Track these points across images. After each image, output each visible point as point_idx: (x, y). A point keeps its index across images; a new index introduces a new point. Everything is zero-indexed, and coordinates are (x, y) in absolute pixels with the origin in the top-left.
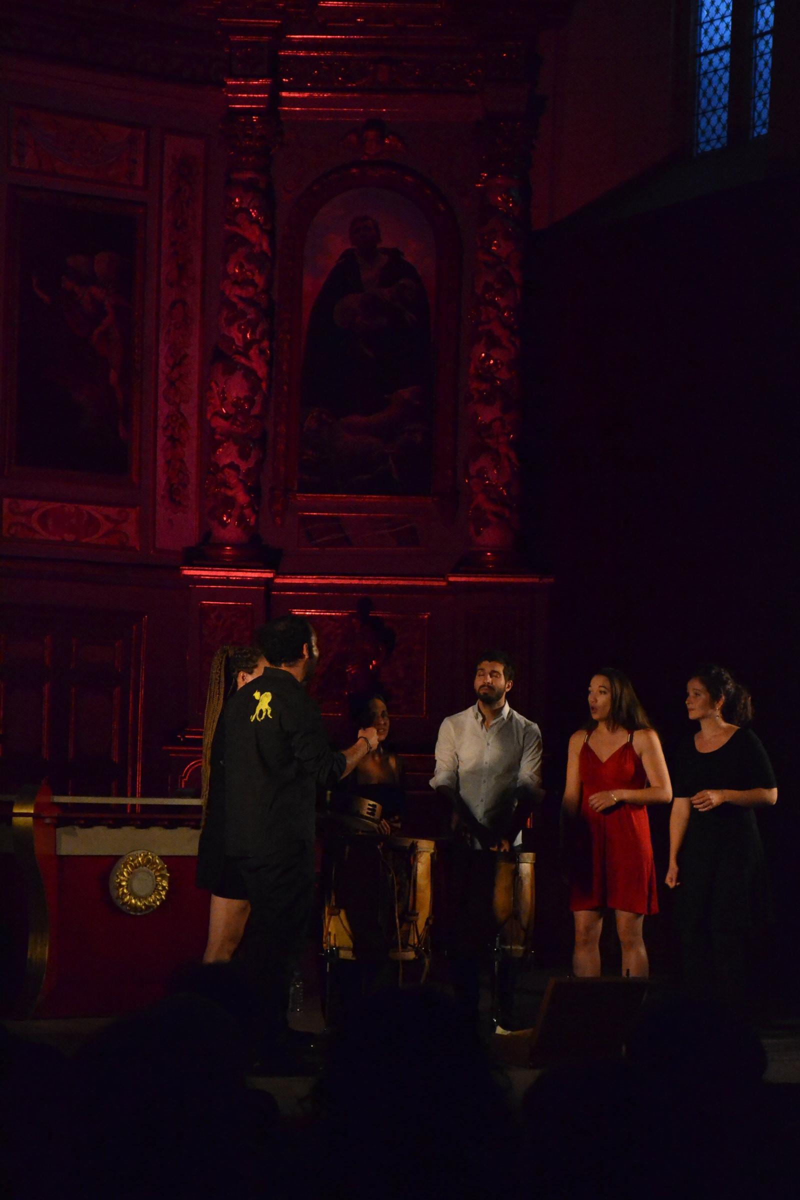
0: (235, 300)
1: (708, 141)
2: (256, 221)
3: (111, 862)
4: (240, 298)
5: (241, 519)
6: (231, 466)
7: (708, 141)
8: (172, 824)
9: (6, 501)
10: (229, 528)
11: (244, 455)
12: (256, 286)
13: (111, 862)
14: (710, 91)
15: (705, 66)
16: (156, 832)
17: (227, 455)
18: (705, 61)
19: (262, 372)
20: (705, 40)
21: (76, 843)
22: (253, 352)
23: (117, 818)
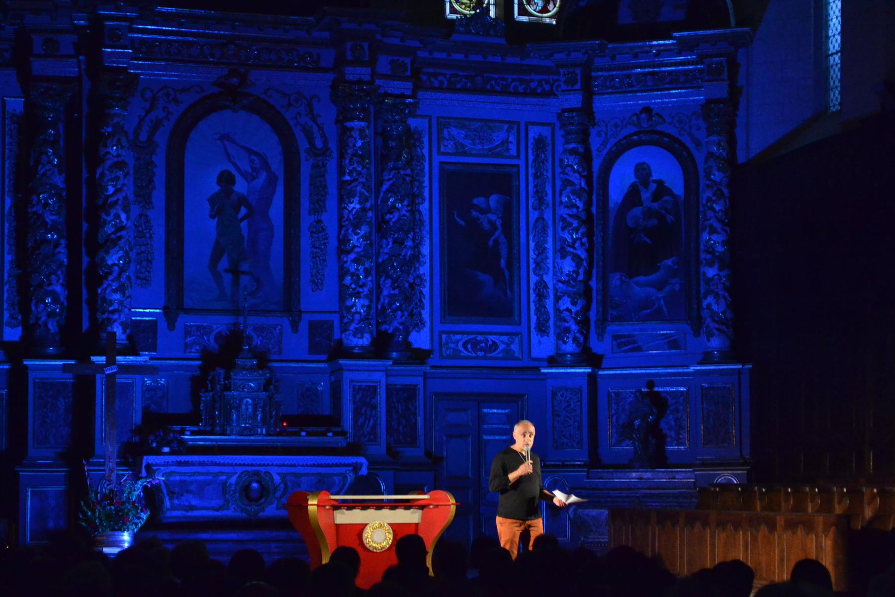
0: (566, 216)
1: (834, 106)
2: (578, 171)
3: (364, 526)
4: (569, 215)
5: (575, 339)
6: (567, 310)
7: (834, 106)
8: (407, 508)
9: (444, 336)
10: (570, 347)
11: (574, 303)
12: (578, 208)
13: (364, 526)
14: (835, 76)
15: (832, 62)
16: (386, 512)
18: (831, 59)
19: (584, 255)
20: (831, 46)
21: (344, 517)
22: (577, 245)
23: (364, 505)
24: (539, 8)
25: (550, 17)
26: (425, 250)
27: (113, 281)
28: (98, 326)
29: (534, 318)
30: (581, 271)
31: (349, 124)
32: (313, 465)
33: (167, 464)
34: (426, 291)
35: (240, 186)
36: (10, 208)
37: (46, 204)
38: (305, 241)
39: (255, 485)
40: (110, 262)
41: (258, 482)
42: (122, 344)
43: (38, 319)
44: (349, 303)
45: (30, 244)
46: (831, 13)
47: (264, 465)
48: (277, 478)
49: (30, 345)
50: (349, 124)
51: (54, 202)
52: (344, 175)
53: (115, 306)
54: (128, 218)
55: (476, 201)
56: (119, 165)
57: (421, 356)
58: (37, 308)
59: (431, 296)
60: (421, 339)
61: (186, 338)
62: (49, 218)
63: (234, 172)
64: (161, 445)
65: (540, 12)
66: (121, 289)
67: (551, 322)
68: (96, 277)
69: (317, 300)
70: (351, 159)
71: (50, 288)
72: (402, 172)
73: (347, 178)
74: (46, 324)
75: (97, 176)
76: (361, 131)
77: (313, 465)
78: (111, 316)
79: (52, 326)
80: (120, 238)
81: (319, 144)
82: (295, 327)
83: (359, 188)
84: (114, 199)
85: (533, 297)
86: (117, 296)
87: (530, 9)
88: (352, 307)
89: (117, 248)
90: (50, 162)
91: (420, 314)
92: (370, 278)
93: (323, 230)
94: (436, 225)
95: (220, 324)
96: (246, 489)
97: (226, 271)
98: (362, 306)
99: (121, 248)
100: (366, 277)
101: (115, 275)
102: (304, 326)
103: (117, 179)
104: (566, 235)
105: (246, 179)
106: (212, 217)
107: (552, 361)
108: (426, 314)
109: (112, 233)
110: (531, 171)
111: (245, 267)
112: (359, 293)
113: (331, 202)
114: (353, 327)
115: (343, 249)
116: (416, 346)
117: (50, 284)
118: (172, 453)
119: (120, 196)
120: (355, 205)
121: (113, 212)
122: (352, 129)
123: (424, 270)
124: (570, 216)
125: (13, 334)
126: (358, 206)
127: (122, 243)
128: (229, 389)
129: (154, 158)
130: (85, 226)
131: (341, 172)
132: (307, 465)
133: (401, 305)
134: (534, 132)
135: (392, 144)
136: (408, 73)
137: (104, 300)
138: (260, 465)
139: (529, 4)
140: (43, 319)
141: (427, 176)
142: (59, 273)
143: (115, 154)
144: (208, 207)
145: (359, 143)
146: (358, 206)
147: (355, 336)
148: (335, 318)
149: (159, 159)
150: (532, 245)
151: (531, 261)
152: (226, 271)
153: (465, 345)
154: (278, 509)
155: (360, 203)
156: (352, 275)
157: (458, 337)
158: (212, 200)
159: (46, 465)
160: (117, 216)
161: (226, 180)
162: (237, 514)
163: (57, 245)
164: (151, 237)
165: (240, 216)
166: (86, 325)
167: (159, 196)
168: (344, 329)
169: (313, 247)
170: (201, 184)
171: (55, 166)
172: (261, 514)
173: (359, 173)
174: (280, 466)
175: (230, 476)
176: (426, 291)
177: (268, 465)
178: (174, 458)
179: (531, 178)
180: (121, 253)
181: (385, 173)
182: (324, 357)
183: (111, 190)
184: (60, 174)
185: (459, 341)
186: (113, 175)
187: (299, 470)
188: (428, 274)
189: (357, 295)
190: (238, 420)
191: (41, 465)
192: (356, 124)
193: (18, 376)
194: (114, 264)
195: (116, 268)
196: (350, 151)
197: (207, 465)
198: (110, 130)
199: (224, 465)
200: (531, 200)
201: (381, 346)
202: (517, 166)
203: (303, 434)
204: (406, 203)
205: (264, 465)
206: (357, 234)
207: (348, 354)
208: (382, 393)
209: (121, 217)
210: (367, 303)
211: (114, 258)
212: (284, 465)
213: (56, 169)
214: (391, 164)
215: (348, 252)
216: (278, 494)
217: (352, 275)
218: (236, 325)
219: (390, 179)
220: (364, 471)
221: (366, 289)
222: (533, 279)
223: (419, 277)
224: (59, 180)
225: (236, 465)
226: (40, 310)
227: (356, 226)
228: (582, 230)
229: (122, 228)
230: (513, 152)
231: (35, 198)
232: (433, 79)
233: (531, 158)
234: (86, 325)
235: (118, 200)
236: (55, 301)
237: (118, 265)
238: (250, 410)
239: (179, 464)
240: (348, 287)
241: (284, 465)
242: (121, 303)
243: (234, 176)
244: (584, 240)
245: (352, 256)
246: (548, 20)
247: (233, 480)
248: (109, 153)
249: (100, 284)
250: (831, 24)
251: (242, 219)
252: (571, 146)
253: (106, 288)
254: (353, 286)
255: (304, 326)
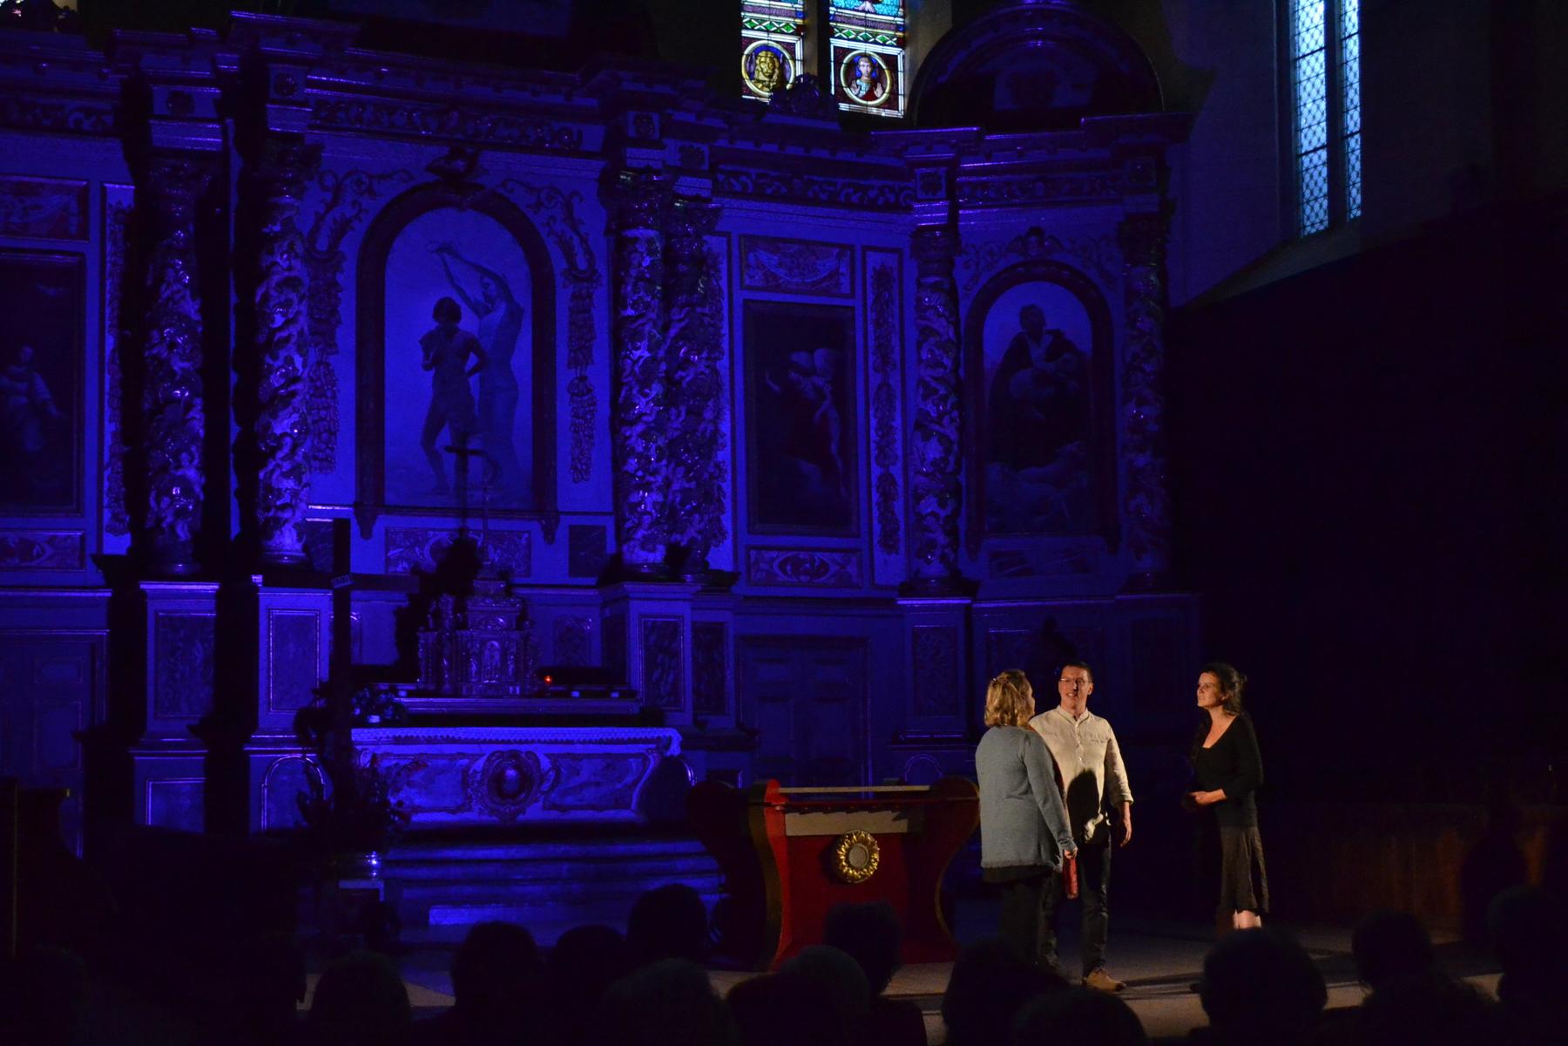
3: (836, 840)
6: (933, 514)
9: (753, 553)
13: (836, 840)
14: (1312, 185)
17: (929, 505)
18: (1306, 159)
24: (863, 93)
25: (878, 106)
26: (725, 427)
27: (283, 459)
28: (259, 531)
29: (877, 528)
30: (951, 458)
31: (630, 233)
32: (600, 742)
33: (377, 742)
34: (727, 487)
35: (468, 323)
36: (113, 351)
37: (173, 345)
38: (564, 409)
39: (511, 773)
40: (278, 431)
41: (516, 767)
42: (290, 557)
43: (160, 520)
44: (634, 498)
45: (147, 406)
46: (1304, 95)
47: (526, 742)
48: (545, 763)
49: (149, 557)
50: (630, 233)
51: (185, 342)
52: (625, 308)
53: (286, 499)
54: (304, 365)
55: (795, 357)
56: (290, 283)
57: (720, 582)
58: (158, 504)
59: (734, 493)
60: (721, 557)
61: (387, 551)
62: (178, 365)
63: (459, 302)
64: (368, 711)
65: (863, 98)
66: (295, 473)
67: (901, 533)
68: (254, 453)
69: (585, 495)
70: (635, 284)
71: (180, 472)
72: (699, 309)
73: (630, 312)
74: (172, 526)
75: (258, 299)
76: (650, 241)
77: (600, 742)
78: (280, 514)
79: (182, 532)
80: (293, 394)
81: (582, 264)
82: (549, 534)
83: (647, 328)
84: (284, 334)
85: (875, 497)
86: (289, 484)
87: (851, 93)
88: (639, 504)
89: (290, 409)
90: (179, 280)
91: (719, 521)
92: (664, 462)
93: (589, 391)
94: (739, 386)
95: (441, 530)
96: (499, 778)
97: (449, 449)
98: (654, 504)
99: (296, 410)
100: (658, 460)
101: (286, 450)
102: (562, 533)
103: (287, 304)
104: (930, 407)
105: (477, 313)
106: (427, 368)
107: (908, 590)
108: (727, 521)
109: (282, 387)
110: (871, 316)
111: (474, 443)
112: (650, 483)
113: (601, 350)
114: (639, 535)
115: (620, 415)
116: (713, 566)
117: (179, 466)
118: (383, 724)
119: (294, 330)
120: (642, 353)
121: (283, 354)
122: (636, 240)
123: (723, 455)
124: (935, 379)
125: (118, 544)
126: (646, 354)
127: (297, 400)
128: (463, 626)
129: (340, 278)
130: (234, 377)
131: (617, 301)
132: (590, 742)
133: (699, 505)
134: (874, 260)
135: (682, 268)
136: (706, 167)
137: (269, 489)
138: (520, 742)
139: (849, 86)
140: (169, 519)
141: (726, 320)
142: (193, 449)
143: (285, 265)
144: (420, 354)
145: (647, 262)
146: (646, 354)
147: (643, 548)
148: (609, 523)
149: (346, 277)
150: (873, 422)
151: (873, 446)
152: (449, 449)
153: (782, 566)
154: (544, 808)
155: (649, 350)
156: (639, 456)
157: (774, 554)
158: (428, 342)
159: (177, 745)
160: (289, 361)
161: (447, 312)
162: (485, 818)
163: (189, 406)
164: (334, 397)
165: (467, 368)
166: (235, 529)
167: (346, 336)
168: (622, 536)
169: (576, 416)
170: (410, 321)
171: (185, 286)
172: (520, 817)
173: (647, 306)
174: (551, 742)
175: (474, 757)
176: (727, 487)
177: (533, 742)
178: (390, 732)
179: (871, 328)
180: (295, 417)
181: (675, 310)
182: (592, 581)
183: (279, 320)
184: (193, 299)
185: (773, 559)
186: (283, 298)
187: (579, 749)
188: (728, 462)
189: (647, 487)
190: (478, 672)
191: (169, 745)
192: (641, 232)
193: (127, 613)
194: (285, 434)
195: (288, 439)
196: (633, 273)
197: (439, 742)
198: (277, 228)
199: (466, 742)
200: (871, 358)
201: (678, 562)
202: (852, 308)
203: (576, 694)
204: (704, 355)
205: (526, 742)
206: (645, 395)
207: (634, 574)
208: (686, 635)
209: (292, 362)
210: (660, 499)
211: (284, 425)
212: (556, 742)
213: (188, 293)
214: (682, 298)
215: (632, 423)
216: (546, 786)
217: (639, 456)
218: (462, 530)
219: (680, 320)
220: (675, 749)
221: (659, 479)
222: (876, 471)
223: (717, 465)
224: (191, 308)
225: (485, 742)
226: (163, 506)
227: (645, 383)
228: (952, 399)
229: (296, 379)
230: (846, 289)
231: (155, 334)
232: (733, 181)
233: (871, 297)
234: (235, 529)
235: (290, 335)
236: (187, 491)
237: (290, 435)
238: (497, 658)
239: (397, 741)
240: (634, 476)
241: (556, 742)
242: (295, 494)
243: (458, 308)
244: (955, 414)
245: (639, 428)
246: (875, 111)
247: (481, 762)
248: (276, 263)
249: (263, 465)
250: (1305, 111)
251: (471, 373)
252: (932, 280)
253: (272, 471)
254: (640, 473)
255: (562, 533)
